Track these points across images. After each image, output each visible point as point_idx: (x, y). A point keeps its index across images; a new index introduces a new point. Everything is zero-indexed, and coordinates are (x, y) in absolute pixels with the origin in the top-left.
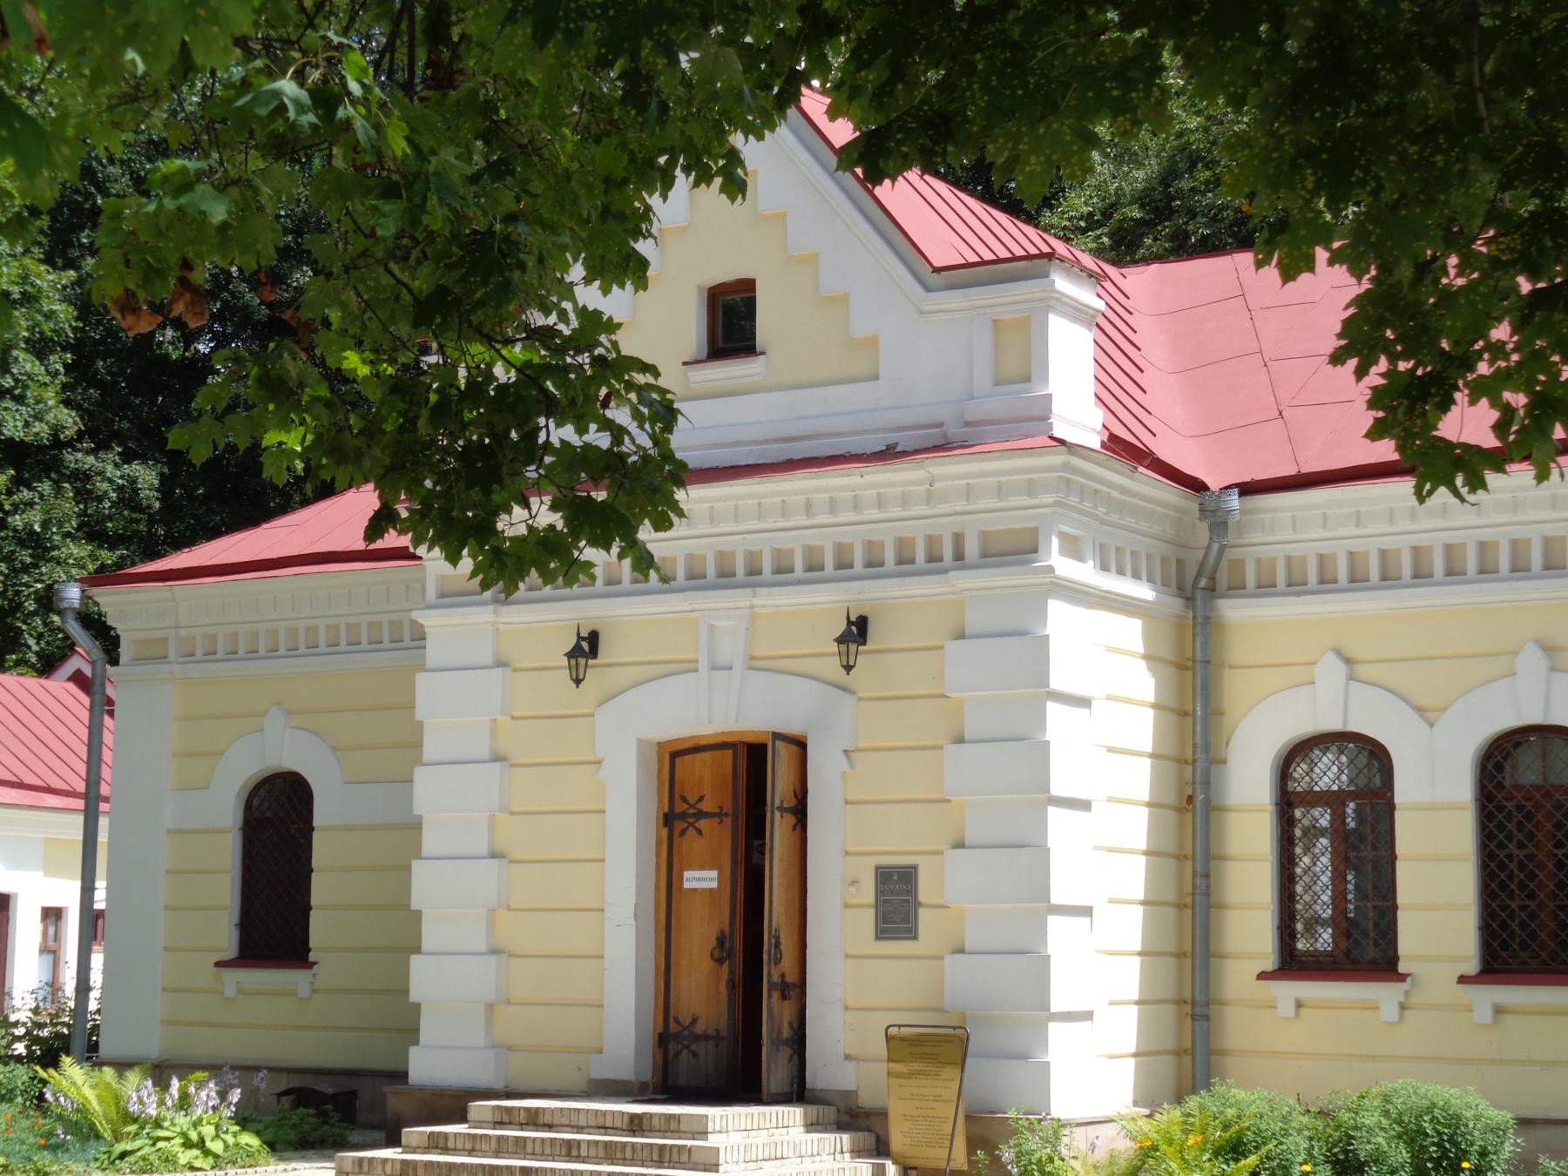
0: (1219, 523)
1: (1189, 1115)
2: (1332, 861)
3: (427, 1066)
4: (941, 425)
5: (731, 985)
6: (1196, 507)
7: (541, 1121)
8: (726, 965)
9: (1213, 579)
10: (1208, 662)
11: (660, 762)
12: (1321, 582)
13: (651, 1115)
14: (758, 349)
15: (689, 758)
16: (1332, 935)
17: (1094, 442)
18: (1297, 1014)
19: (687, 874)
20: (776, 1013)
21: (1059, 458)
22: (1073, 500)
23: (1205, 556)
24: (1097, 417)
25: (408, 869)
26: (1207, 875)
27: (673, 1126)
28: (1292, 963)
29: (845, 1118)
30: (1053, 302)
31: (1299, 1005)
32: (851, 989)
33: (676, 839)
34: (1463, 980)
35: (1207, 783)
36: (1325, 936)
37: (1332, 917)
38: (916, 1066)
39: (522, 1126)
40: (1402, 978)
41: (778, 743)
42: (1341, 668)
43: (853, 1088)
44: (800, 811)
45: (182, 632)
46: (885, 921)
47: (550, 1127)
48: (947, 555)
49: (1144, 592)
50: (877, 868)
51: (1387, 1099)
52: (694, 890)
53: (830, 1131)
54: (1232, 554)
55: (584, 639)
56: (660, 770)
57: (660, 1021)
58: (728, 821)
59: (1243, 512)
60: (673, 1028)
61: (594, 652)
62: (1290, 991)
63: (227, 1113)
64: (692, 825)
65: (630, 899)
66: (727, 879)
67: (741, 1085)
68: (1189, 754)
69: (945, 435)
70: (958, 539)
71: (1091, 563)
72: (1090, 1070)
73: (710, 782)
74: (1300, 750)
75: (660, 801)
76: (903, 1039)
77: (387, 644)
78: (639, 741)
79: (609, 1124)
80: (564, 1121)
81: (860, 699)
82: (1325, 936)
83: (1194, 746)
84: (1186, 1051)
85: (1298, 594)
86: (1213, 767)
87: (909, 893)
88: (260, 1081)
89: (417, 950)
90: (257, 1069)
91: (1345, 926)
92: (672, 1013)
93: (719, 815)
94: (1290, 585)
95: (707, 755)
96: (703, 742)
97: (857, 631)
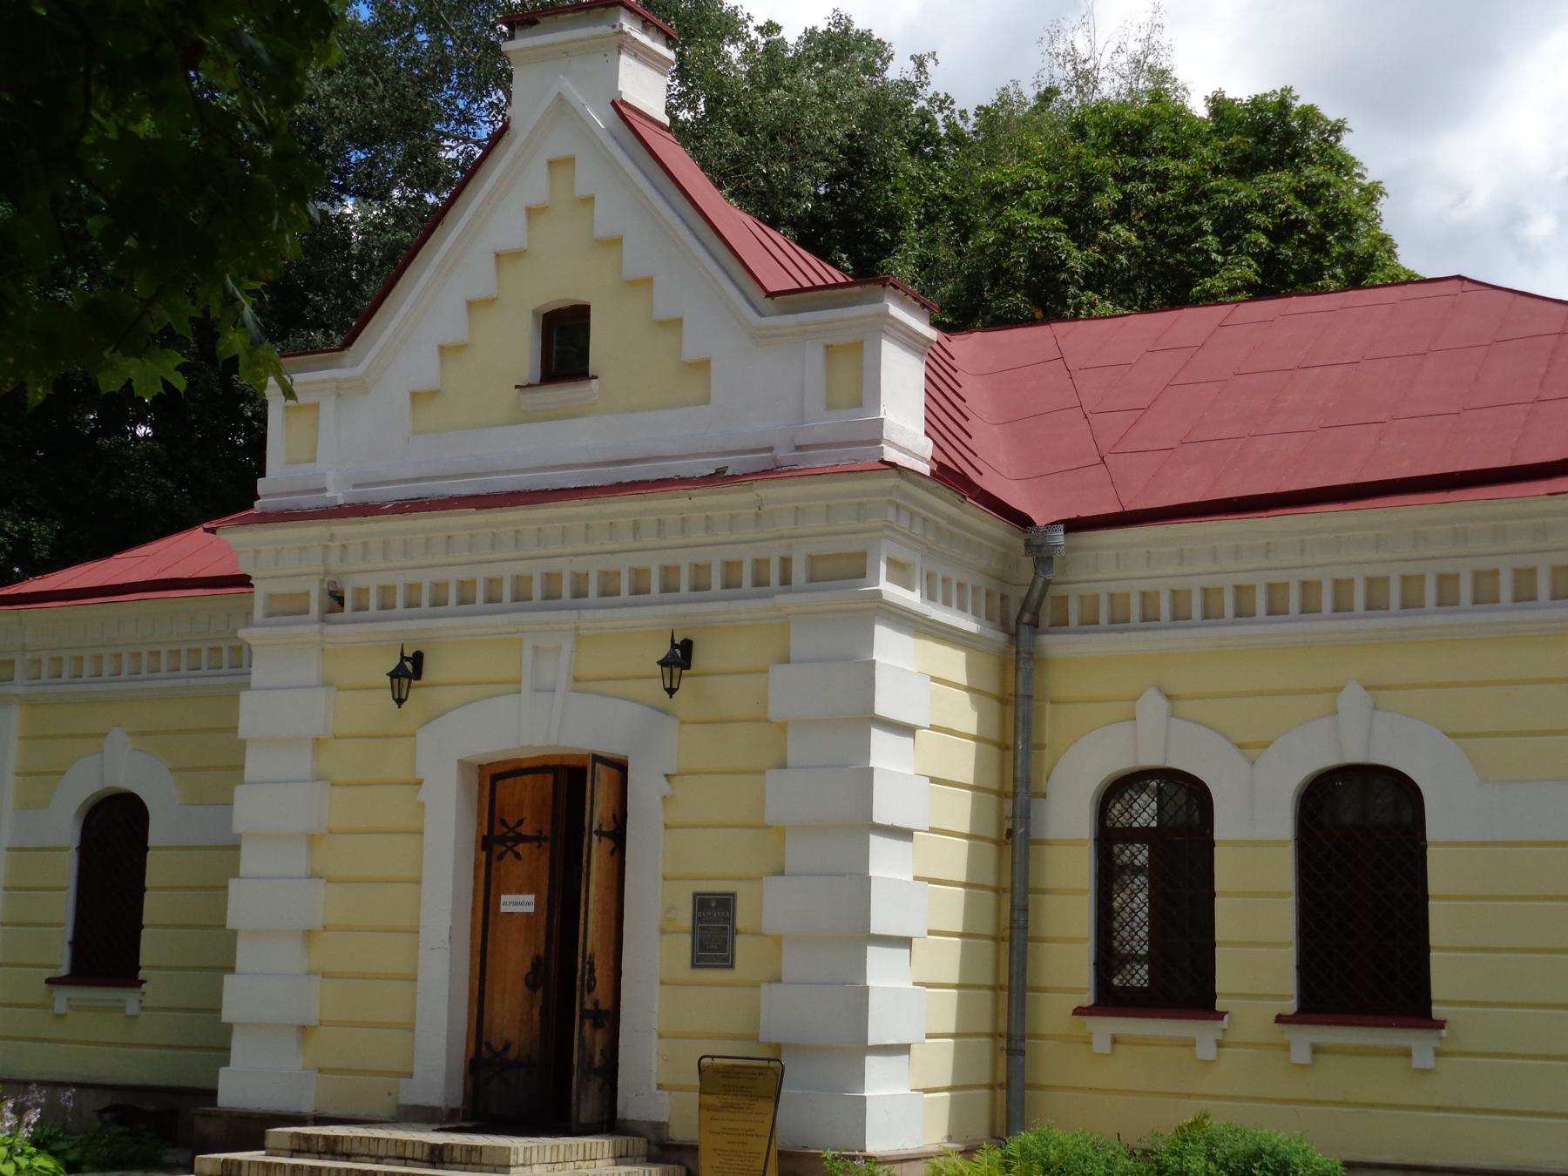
0: (1042, 558)
1: (1010, 1157)
2: (1149, 896)
3: (238, 1088)
4: (770, 449)
5: (544, 1011)
6: (1021, 543)
7: (339, 1149)
8: (540, 993)
9: (1036, 614)
10: (1030, 697)
11: (481, 785)
12: (1144, 620)
13: (452, 1147)
14: (591, 373)
15: (509, 781)
16: (1148, 972)
17: (925, 469)
18: (1113, 1050)
19: (504, 898)
20: (587, 1041)
21: (890, 481)
22: (904, 522)
23: (1030, 592)
24: (926, 447)
25: (226, 888)
26: (1026, 910)
27: (475, 1158)
28: (1110, 999)
29: (655, 1150)
30: (886, 327)
31: (1115, 1040)
32: (665, 1021)
33: (495, 864)
34: (1281, 1019)
35: (1027, 818)
36: (1142, 972)
37: (1149, 953)
38: (729, 1099)
39: (320, 1155)
40: (1220, 1016)
41: (598, 765)
42: (1163, 704)
43: (665, 1119)
44: (618, 835)
45: (29, 656)
46: (703, 947)
47: (348, 1156)
48: (770, 577)
49: (968, 624)
50: (695, 895)
51: (1211, 1143)
52: (511, 914)
53: (640, 1164)
54: (1054, 591)
55: (408, 659)
56: (481, 793)
57: (472, 1045)
58: (546, 845)
59: (1069, 549)
60: (485, 1053)
61: (417, 673)
62: (1105, 1028)
63: (24, 1133)
64: (511, 848)
65: (447, 923)
66: (544, 905)
67: (549, 1115)
68: (1009, 787)
69: (774, 459)
70: (786, 562)
71: (918, 591)
72: (905, 1100)
73: (526, 801)
74: (1119, 788)
75: (480, 824)
76: (717, 1071)
77: (226, 669)
78: (461, 762)
79: (408, 1154)
80: (363, 1150)
81: (683, 722)
82: (1142, 972)
83: (1015, 780)
84: (1001, 1085)
85: (1122, 631)
86: (1034, 802)
87: (727, 920)
88: (67, 1098)
89: (232, 970)
90: (65, 1085)
91: (1159, 957)
92: (485, 1039)
93: (538, 838)
94: (1112, 622)
95: (528, 779)
96: (525, 765)
97: (680, 657)
